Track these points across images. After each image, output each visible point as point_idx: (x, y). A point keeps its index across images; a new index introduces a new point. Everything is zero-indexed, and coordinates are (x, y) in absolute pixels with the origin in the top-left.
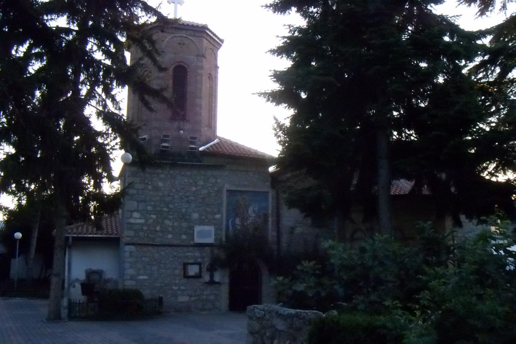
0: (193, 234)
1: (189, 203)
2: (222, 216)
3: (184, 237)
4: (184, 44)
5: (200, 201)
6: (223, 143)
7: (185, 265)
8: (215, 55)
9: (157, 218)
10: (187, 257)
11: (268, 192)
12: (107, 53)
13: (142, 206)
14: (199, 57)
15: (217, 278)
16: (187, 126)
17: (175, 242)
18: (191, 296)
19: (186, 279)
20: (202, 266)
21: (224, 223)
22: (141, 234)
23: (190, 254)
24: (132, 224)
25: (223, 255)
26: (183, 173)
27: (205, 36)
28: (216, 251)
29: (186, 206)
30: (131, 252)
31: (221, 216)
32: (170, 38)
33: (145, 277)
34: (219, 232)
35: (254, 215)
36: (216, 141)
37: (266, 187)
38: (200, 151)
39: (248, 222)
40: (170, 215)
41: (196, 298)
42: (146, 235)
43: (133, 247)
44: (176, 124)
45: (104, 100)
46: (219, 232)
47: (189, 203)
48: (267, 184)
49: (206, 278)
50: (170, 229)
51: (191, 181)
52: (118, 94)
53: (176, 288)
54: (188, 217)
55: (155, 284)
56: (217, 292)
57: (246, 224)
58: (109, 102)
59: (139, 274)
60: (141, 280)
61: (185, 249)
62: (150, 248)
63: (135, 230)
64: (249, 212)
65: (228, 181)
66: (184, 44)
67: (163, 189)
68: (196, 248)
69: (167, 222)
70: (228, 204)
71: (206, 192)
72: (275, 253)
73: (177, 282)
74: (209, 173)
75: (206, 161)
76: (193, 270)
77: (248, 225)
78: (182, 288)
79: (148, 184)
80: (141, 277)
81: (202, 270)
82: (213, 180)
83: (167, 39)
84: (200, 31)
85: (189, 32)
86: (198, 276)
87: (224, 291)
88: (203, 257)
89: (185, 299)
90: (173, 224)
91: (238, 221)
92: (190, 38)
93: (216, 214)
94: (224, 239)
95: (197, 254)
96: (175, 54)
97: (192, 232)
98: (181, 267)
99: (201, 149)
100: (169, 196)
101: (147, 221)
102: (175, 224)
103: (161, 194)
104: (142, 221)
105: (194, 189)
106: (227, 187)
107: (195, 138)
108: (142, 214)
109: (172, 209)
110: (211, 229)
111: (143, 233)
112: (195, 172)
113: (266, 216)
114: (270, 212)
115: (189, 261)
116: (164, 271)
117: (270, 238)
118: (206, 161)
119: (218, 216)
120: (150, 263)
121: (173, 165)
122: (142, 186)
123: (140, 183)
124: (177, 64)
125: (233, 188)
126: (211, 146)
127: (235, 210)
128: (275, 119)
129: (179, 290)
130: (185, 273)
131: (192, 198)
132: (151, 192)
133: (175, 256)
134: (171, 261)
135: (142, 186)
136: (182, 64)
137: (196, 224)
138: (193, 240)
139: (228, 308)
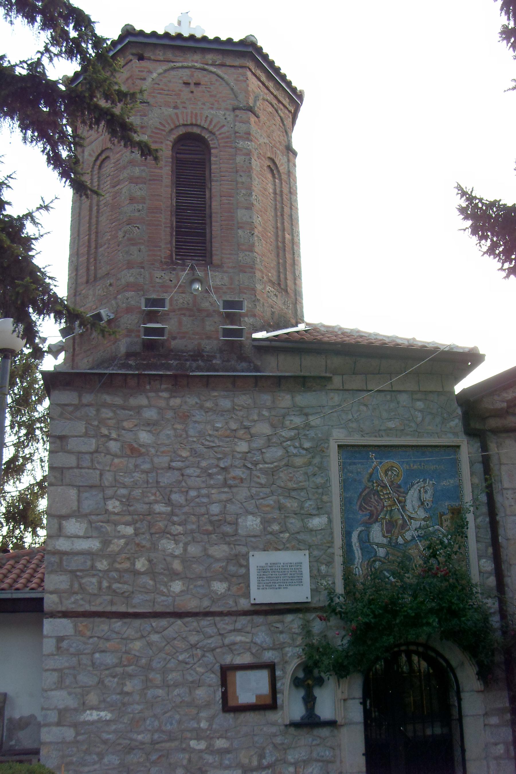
0: (246, 577)
1: (230, 487)
2: (330, 521)
4: (197, 84)
5: (263, 481)
7: (226, 673)
10: (231, 647)
11: (458, 447)
13: (90, 502)
14: (237, 112)
15: (326, 706)
16: (215, 278)
17: (192, 605)
19: (230, 716)
20: (278, 673)
21: (338, 541)
22: (91, 582)
23: (239, 638)
24: (66, 553)
25: (339, 638)
26: (209, 404)
27: (251, 65)
28: (317, 626)
29: (224, 497)
30: (60, 639)
32: (160, 71)
34: (323, 568)
35: (422, 514)
37: (450, 432)
40: (174, 523)
42: (105, 584)
43: (65, 621)
44: (184, 275)
46: (323, 568)
47: (230, 487)
48: (452, 424)
49: (293, 708)
50: (177, 565)
51: (233, 426)
52: (38, 229)
53: (202, 745)
54: (228, 529)
55: (135, 736)
56: (328, 754)
57: (400, 540)
59: (84, 706)
60: (93, 723)
61: (225, 624)
62: (117, 624)
63: (73, 572)
64: (409, 507)
65: (339, 420)
66: (197, 84)
67: (152, 451)
68: (259, 619)
69: (168, 545)
70: (346, 484)
71: (280, 452)
72: (495, 621)
73: (203, 725)
74: (285, 400)
75: (273, 366)
76: (251, 687)
78: (220, 743)
79: (108, 438)
80: (92, 716)
81: (279, 685)
82: (298, 421)
83: (155, 75)
85: (210, 57)
86: (270, 704)
90: (185, 550)
94: (340, 589)
95: (262, 637)
97: (243, 571)
98: (214, 679)
100: (170, 468)
101: (106, 543)
102: (193, 550)
103: (146, 466)
104: (94, 544)
105: (243, 447)
106: (339, 436)
107: (238, 305)
108: (90, 523)
109: (181, 506)
110: (301, 558)
111: (94, 580)
112: (243, 399)
113: (457, 513)
114: (468, 497)
115: (239, 660)
116: (160, 692)
117: (475, 577)
119: (317, 522)
120: (119, 670)
121: (180, 382)
122: (92, 444)
123: (86, 435)
124: (181, 131)
125: (357, 440)
127: (364, 502)
129: (210, 750)
130: (225, 696)
131: (239, 473)
132: (116, 461)
133: (194, 646)
134: (181, 662)
135: (92, 444)
136: (196, 130)
137: (255, 548)
138: (247, 595)
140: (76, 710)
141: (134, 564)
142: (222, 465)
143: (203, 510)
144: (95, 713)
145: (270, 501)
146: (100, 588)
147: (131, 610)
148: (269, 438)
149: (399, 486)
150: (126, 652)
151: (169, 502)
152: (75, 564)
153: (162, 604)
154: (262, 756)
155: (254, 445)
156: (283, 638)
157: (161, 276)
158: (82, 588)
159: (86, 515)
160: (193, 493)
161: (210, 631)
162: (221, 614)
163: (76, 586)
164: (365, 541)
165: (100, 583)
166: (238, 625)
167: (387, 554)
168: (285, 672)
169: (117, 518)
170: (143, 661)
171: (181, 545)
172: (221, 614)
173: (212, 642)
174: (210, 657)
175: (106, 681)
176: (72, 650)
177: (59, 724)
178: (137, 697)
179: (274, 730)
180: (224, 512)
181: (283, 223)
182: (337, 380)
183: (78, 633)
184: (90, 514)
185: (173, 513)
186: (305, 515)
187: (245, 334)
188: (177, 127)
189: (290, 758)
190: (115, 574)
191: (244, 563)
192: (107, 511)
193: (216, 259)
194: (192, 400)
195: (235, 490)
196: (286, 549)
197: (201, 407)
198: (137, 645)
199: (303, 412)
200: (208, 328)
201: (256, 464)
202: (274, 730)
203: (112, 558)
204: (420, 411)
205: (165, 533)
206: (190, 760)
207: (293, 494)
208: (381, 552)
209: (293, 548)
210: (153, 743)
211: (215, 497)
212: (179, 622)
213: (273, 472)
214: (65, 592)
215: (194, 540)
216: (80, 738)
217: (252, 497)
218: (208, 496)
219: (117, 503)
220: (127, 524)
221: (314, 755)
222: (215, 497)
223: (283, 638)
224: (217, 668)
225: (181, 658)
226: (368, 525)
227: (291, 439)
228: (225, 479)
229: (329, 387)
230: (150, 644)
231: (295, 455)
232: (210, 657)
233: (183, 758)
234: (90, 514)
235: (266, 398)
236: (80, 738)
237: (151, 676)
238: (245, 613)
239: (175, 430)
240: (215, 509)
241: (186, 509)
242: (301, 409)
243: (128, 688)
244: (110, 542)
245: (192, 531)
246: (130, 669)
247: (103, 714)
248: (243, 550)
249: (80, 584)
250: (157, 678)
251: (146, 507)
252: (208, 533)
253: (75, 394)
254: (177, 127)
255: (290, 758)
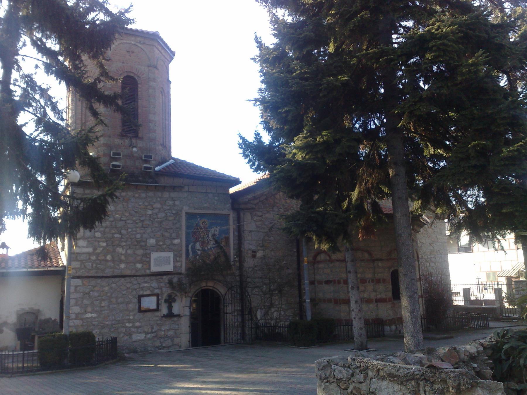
0: (149, 262)
1: (144, 228)
2: (181, 241)
3: (139, 266)
4: (133, 52)
6: (179, 163)
8: (166, 67)
9: (107, 246)
10: (142, 288)
12: (433, 46)
16: (140, 144)
17: (128, 272)
18: (147, 333)
19: (141, 314)
20: (160, 297)
23: (146, 285)
26: (137, 195)
27: (156, 44)
29: (142, 231)
30: (76, 287)
31: (180, 241)
33: (94, 315)
34: (178, 258)
36: (171, 161)
37: (226, 209)
38: (157, 171)
39: (209, 247)
40: (122, 242)
41: (153, 335)
42: (94, 265)
44: (127, 141)
45: (44, 108)
46: (178, 258)
47: (144, 228)
48: (228, 206)
49: (164, 310)
50: (123, 257)
51: (146, 204)
53: (131, 325)
54: (143, 244)
56: (176, 327)
57: (206, 248)
58: (49, 110)
59: (86, 312)
61: (140, 280)
62: (99, 281)
63: (81, 261)
65: (185, 203)
66: (133, 52)
68: (153, 278)
69: (120, 250)
70: (188, 228)
71: (164, 215)
73: (131, 317)
74: (166, 195)
77: (208, 249)
78: (137, 324)
80: (89, 315)
81: (160, 302)
82: (171, 203)
84: (152, 39)
87: (185, 325)
88: (160, 288)
89: (142, 336)
90: (126, 251)
91: (198, 246)
92: (140, 46)
93: (174, 239)
95: (155, 284)
96: (123, 63)
97: (148, 259)
98: (135, 300)
99: (157, 169)
101: (95, 249)
104: (90, 250)
105: (150, 212)
106: (186, 209)
108: (89, 241)
110: (170, 255)
111: (90, 264)
112: (151, 194)
115: (145, 293)
116: (115, 306)
118: (164, 181)
119: (176, 241)
120: (100, 298)
124: (125, 74)
125: (192, 211)
126: (167, 166)
127: (194, 234)
128: (241, 138)
129: (133, 327)
136: (132, 75)
137: (153, 251)
138: (149, 269)
139: (188, 344)
140: (82, 314)
141: (106, 257)
142: (142, 219)
143: (133, 236)
144: (90, 314)
145: (159, 233)
146: (92, 267)
147: (104, 275)
148: (160, 209)
149: (207, 228)
150: (103, 291)
151: (120, 233)
152: (82, 258)
153: (117, 272)
154: (152, 328)
155: (154, 212)
156: (162, 285)
157: (117, 141)
158: (85, 267)
159: (87, 239)
160: (130, 230)
161: (135, 282)
162: (139, 276)
163: (83, 266)
164: (193, 248)
165: (92, 265)
166: (146, 280)
167: (201, 253)
168: (162, 298)
169: (99, 239)
170: (109, 294)
171: (125, 250)
172: (139, 276)
173: (136, 287)
174: (134, 293)
175: (95, 302)
176: (81, 291)
177: (76, 319)
178: (106, 308)
179: (157, 318)
180: (142, 237)
181: (165, 117)
182: (186, 187)
183: (83, 284)
184: (89, 238)
185: (122, 238)
186: (171, 238)
187: (152, 169)
188: (124, 72)
189: (163, 329)
190: (98, 261)
191: (149, 256)
192: (95, 237)
193: (140, 135)
194: (130, 194)
195: (146, 229)
196: (164, 251)
197: (134, 196)
198: (106, 289)
199: (173, 199)
200: (137, 164)
201: (154, 219)
202: (157, 318)
203: (98, 255)
204: (216, 200)
205: (119, 245)
206: (126, 331)
207: (168, 231)
208: (199, 253)
209: (167, 251)
210: (112, 325)
211: (138, 231)
212: (123, 279)
213: (161, 222)
214: (78, 268)
215: (130, 248)
216: (84, 324)
217: (152, 232)
218: (136, 231)
219: (99, 234)
220: (103, 242)
221: (172, 327)
222: (138, 231)
223: (162, 285)
224: (137, 296)
225: (123, 293)
226: (195, 243)
227: (168, 210)
228: (143, 225)
229: (183, 190)
230: (111, 288)
231: (170, 216)
232: (134, 293)
233: (123, 330)
234: (89, 238)
235: (159, 194)
236: (84, 324)
237: (112, 300)
238: (149, 275)
239: (123, 205)
240: (138, 236)
241: (127, 236)
242: (173, 198)
243: (103, 304)
244: (97, 249)
245: (129, 245)
246: (104, 297)
247: (93, 314)
248: (148, 252)
249: (84, 266)
250: (114, 300)
251: (111, 235)
252: (136, 245)
253: (82, 190)
254: (124, 72)
255: (163, 329)
